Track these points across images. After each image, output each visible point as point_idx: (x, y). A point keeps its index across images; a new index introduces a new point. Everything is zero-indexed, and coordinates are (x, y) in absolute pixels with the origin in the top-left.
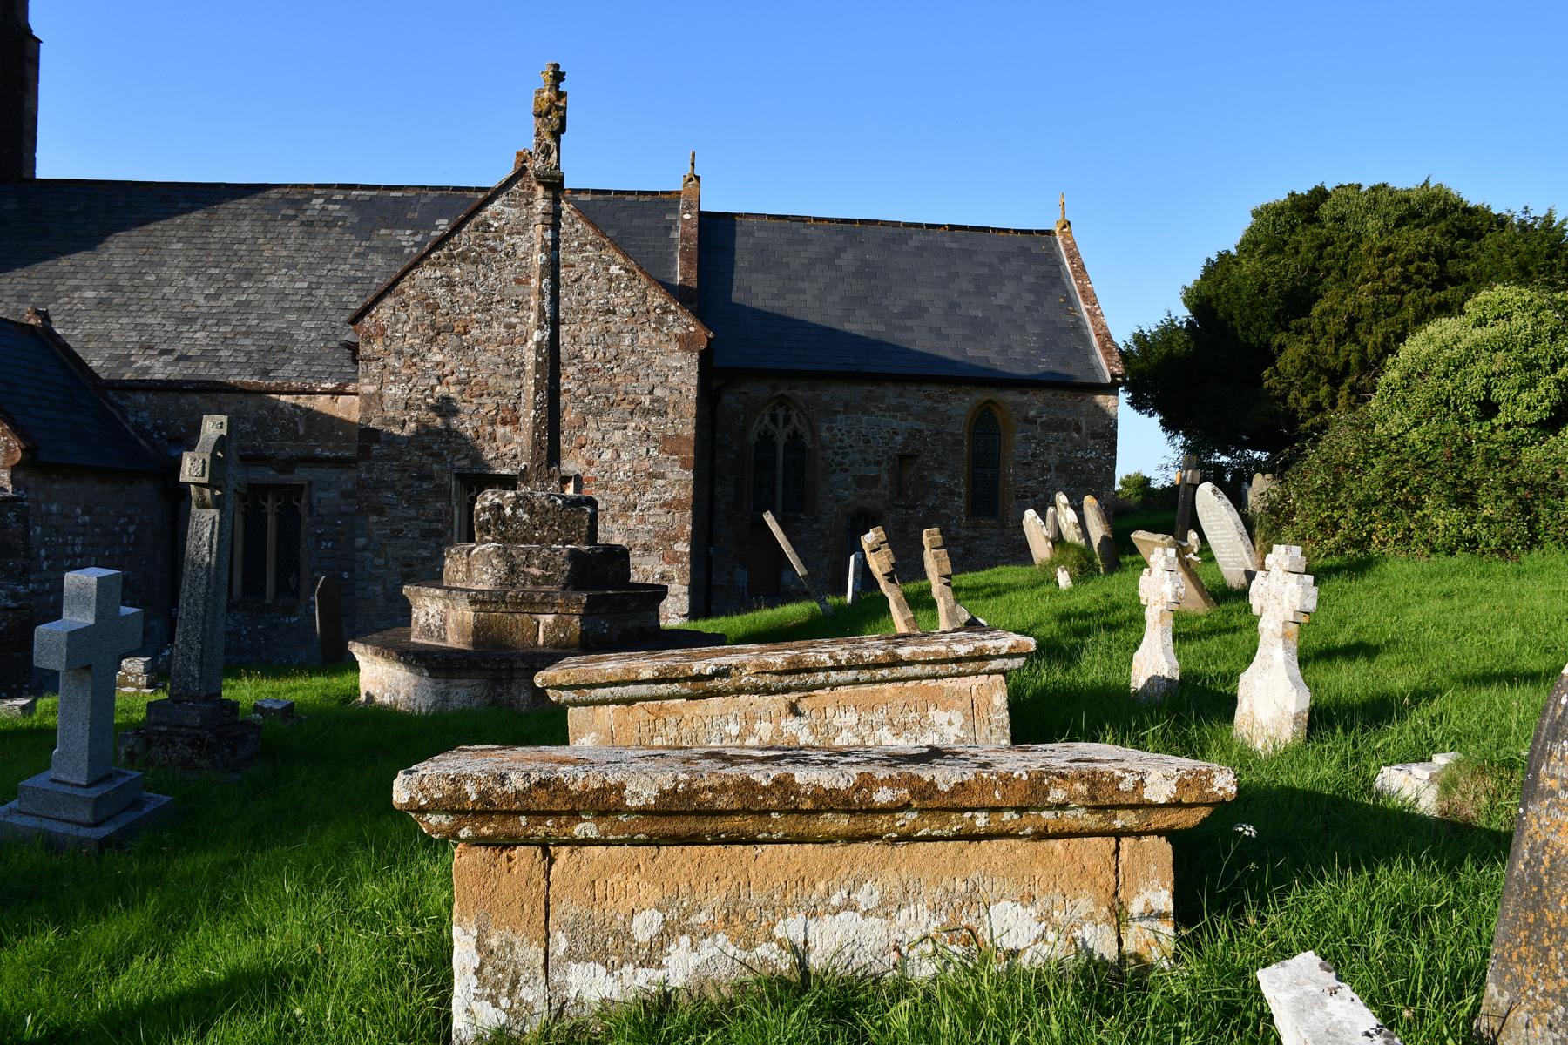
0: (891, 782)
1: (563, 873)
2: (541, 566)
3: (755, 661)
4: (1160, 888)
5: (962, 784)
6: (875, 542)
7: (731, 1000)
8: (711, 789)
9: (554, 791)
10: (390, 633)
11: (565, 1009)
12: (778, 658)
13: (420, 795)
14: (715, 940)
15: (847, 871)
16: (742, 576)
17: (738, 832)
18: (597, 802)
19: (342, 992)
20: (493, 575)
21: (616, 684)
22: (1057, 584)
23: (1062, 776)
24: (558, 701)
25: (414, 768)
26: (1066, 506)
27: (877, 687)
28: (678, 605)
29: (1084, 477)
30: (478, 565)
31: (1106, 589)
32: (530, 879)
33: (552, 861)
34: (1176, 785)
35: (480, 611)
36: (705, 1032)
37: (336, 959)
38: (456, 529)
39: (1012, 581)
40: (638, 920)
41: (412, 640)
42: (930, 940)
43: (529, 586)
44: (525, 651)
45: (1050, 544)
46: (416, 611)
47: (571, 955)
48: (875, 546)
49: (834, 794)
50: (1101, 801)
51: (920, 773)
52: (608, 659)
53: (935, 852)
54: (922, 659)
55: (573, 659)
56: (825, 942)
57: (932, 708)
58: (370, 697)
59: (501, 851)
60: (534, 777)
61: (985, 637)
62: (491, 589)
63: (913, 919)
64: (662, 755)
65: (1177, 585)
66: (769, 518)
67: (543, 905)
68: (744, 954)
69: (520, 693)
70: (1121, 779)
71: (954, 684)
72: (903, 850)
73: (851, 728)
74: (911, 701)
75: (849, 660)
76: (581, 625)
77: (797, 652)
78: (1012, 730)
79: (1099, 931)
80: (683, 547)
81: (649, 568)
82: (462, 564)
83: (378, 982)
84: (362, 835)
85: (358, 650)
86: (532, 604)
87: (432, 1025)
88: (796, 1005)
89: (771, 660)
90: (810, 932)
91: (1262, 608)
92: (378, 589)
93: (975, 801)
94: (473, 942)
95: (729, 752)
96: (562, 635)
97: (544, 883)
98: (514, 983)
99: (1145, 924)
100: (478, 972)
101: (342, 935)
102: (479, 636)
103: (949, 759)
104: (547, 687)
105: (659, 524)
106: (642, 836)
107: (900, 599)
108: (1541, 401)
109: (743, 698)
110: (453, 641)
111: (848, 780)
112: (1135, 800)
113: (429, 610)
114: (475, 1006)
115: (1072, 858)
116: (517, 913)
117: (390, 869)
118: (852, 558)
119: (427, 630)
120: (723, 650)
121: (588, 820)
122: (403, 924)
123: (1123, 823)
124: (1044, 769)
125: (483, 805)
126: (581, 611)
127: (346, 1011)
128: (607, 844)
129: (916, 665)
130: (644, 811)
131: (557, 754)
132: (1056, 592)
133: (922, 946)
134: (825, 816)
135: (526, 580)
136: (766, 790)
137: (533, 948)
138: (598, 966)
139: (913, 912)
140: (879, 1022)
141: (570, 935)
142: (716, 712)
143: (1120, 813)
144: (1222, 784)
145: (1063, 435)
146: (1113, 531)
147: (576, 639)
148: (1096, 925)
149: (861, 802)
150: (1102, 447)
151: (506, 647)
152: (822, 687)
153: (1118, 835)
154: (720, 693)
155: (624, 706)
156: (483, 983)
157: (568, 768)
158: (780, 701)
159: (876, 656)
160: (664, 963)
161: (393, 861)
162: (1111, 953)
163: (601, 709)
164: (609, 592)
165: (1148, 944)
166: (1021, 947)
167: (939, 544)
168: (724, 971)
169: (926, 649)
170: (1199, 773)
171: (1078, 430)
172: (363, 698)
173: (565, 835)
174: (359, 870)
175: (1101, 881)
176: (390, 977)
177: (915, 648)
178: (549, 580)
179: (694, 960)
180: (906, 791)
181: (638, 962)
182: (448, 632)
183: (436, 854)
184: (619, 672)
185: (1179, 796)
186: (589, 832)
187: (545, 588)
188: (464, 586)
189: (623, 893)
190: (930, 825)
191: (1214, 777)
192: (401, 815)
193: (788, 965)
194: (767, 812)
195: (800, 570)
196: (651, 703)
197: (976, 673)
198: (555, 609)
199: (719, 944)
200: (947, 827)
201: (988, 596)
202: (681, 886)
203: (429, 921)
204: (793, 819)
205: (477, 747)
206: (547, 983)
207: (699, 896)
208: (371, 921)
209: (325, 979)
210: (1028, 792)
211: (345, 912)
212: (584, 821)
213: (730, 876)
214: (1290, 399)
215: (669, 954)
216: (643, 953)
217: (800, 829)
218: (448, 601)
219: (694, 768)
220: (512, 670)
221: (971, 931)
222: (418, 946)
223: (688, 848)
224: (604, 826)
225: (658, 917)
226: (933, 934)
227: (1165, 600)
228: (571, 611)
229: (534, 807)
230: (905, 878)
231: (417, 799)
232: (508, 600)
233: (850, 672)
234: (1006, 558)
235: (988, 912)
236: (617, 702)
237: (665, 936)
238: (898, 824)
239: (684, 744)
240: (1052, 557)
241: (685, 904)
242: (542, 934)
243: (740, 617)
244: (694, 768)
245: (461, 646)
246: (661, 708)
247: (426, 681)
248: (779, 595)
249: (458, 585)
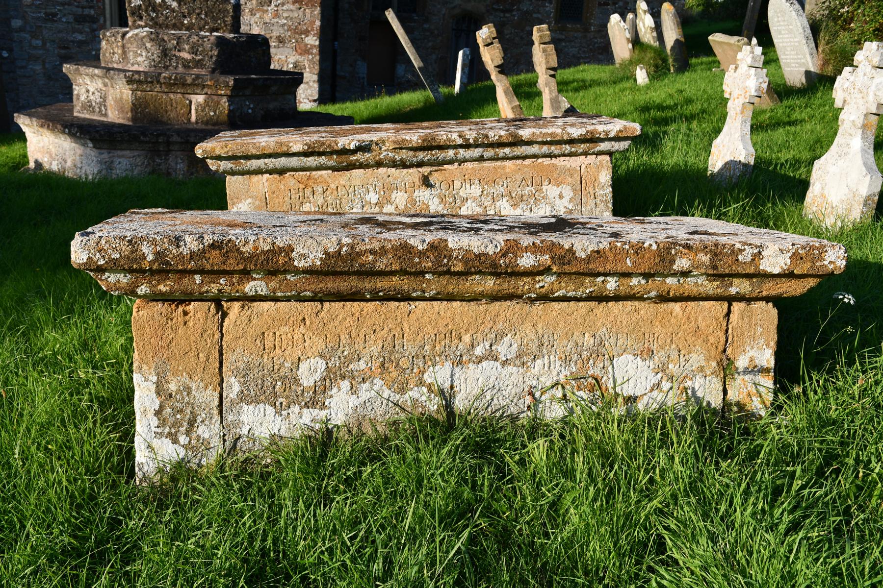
0: (534, 249)
1: (235, 325)
2: (191, 51)
3: (393, 138)
4: (765, 347)
5: (598, 252)
6: (489, 37)
7: (385, 435)
8: (372, 252)
9: (227, 252)
10: (53, 108)
11: (239, 444)
12: (414, 135)
13: (98, 255)
14: (373, 385)
15: (490, 326)
16: (362, 68)
17: (395, 290)
18: (268, 263)
19: (29, 431)
20: (147, 57)
21: (270, 156)
22: (635, 80)
23: (688, 247)
24: (217, 171)
25: (90, 229)
26: (645, 12)
27: (499, 163)
28: (309, 92)
30: (132, 47)
31: (678, 86)
32: (205, 331)
33: (225, 315)
34: (790, 258)
35: (137, 90)
36: (365, 465)
37: (21, 399)
38: (108, 15)
39: (596, 78)
40: (304, 367)
41: (75, 114)
42: (560, 386)
43: (181, 69)
44: (179, 127)
45: (630, 46)
46: (77, 88)
47: (243, 397)
48: (489, 41)
49: (483, 258)
50: (721, 270)
51: (560, 240)
52: (260, 134)
53: (569, 310)
54: (540, 140)
55: (228, 133)
56: (469, 386)
57: (546, 183)
58: (38, 164)
59: (177, 306)
60: (208, 239)
61: (594, 121)
62: (146, 70)
63: (546, 368)
64: (322, 220)
65: (761, 80)
66: (391, 16)
67: (217, 354)
68: (398, 396)
69: (177, 163)
70: (741, 251)
71: (566, 163)
72: (540, 308)
73: (475, 198)
74: (528, 177)
75: (476, 140)
76: (229, 105)
77: (429, 131)
78: (614, 204)
79: (707, 382)
80: (312, 41)
81: (283, 58)
82: (117, 46)
83: (63, 421)
84: (40, 287)
85: (23, 122)
86: (184, 85)
87: (115, 459)
88: (445, 442)
89: (407, 138)
90: (456, 378)
91: (845, 101)
92: (38, 68)
93: (608, 267)
94: (153, 387)
95: (381, 218)
96: (212, 114)
97: (217, 335)
98: (192, 423)
99: (748, 378)
100: (158, 413)
101: (26, 378)
102: (137, 113)
103: (578, 228)
104: (207, 158)
105: (291, 19)
106: (308, 293)
107: (508, 88)
109: (382, 170)
110: (114, 116)
111: (496, 246)
112: (752, 270)
113: (89, 88)
114: (156, 443)
115: (689, 318)
116: (193, 360)
117: (69, 318)
118: (461, 53)
119: (88, 106)
120: (362, 128)
121: (258, 279)
122: (84, 368)
123: (738, 290)
124: (670, 240)
125: (159, 265)
126: (229, 93)
127: (33, 449)
128: (276, 300)
129: (535, 145)
130: (310, 272)
131: (225, 218)
132: (636, 88)
133: (554, 391)
134: (473, 277)
135: (178, 63)
136: (422, 254)
137: (209, 392)
138: (268, 407)
139: (546, 362)
140: (517, 457)
141: (242, 380)
142: (357, 182)
143: (736, 281)
144: (833, 258)
146: (685, 35)
147: (224, 118)
148: (705, 377)
149: (507, 266)
151: (162, 123)
152: (451, 162)
153: (730, 300)
154: (362, 166)
155: (276, 176)
156: (163, 423)
157: (238, 231)
158: (413, 175)
159: (500, 136)
160: (327, 404)
161: (70, 311)
162: (716, 401)
163: (255, 178)
164: (253, 76)
165: (749, 395)
166: (639, 394)
167: (548, 39)
168: (380, 411)
169: (544, 131)
170: (812, 248)
172: (32, 165)
173: (237, 292)
174: (39, 319)
175: (712, 339)
176: (74, 417)
177: (534, 130)
178: (198, 64)
179: (353, 401)
180: (547, 257)
181: (303, 403)
182: (109, 108)
183: (111, 304)
184: (272, 145)
185: (792, 268)
186: (259, 289)
187: (195, 71)
188: (120, 67)
189: (290, 343)
190: (567, 287)
191: (826, 251)
192: (77, 273)
193: (436, 406)
194: (422, 273)
195: (416, 62)
196: (301, 173)
197: (586, 154)
198: (206, 90)
199: (376, 388)
200: (581, 289)
201: (576, 90)
202: (342, 338)
203: (108, 365)
204: (444, 280)
205: (147, 210)
206: (222, 422)
207: (359, 346)
208: (52, 364)
209: (11, 419)
210: (657, 261)
211: (28, 357)
212: (255, 279)
213: (386, 329)
215: (331, 396)
216: (308, 396)
217: (450, 288)
218: (107, 80)
219: (354, 232)
220: (168, 143)
221: (596, 379)
222: (99, 387)
223: (348, 304)
224: (273, 284)
225: (322, 365)
226: (563, 380)
227: (748, 94)
228: (220, 92)
229: (208, 267)
230: (540, 332)
231: (95, 259)
232: (162, 81)
233: (477, 150)
234: (586, 58)
235: (612, 364)
236: (271, 172)
237: (328, 381)
238: (538, 286)
239: (330, 210)
240: (632, 57)
241: (346, 353)
242: (217, 380)
243: (363, 103)
244: (354, 232)
245: (121, 121)
246: (309, 178)
247: (91, 151)
248: (395, 86)
249: (115, 66)
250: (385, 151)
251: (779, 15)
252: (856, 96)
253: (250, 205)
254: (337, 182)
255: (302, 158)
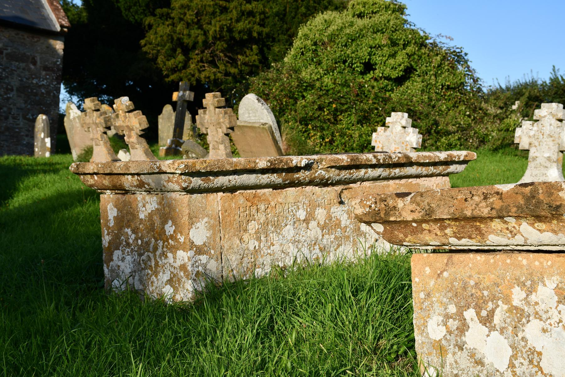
29: (37, 98)
75: (384, 160)
107: (147, 150)
108: (400, 65)
109: (309, 188)
142: (291, 200)
145: (23, 65)
150: (51, 78)
158: (330, 192)
159: (399, 158)
163: (212, 196)
171: (35, 63)
214: (159, 60)
250: (321, 169)
251: (251, 112)
252: (546, 139)
253: (207, 224)
254: (276, 199)
255: (259, 175)
